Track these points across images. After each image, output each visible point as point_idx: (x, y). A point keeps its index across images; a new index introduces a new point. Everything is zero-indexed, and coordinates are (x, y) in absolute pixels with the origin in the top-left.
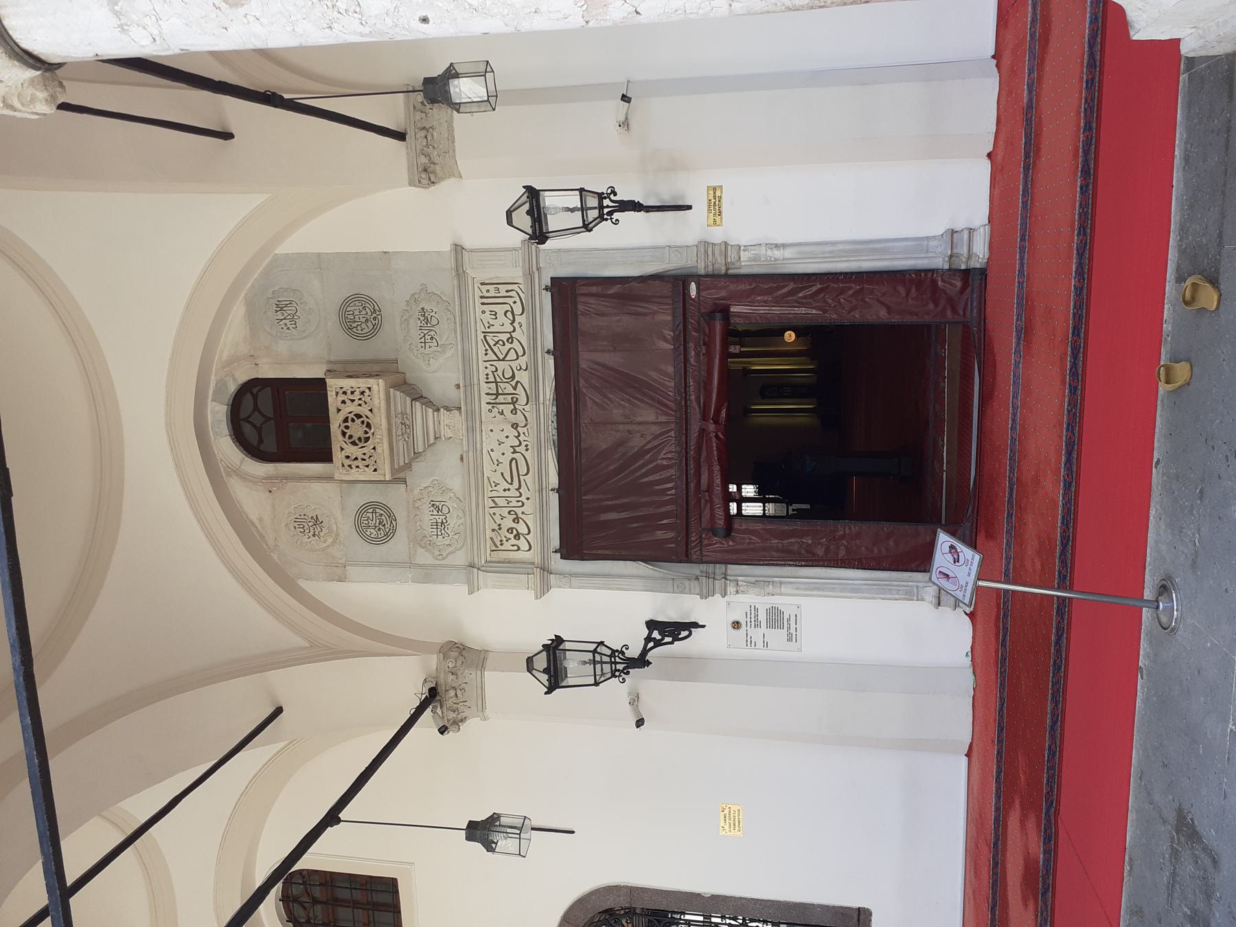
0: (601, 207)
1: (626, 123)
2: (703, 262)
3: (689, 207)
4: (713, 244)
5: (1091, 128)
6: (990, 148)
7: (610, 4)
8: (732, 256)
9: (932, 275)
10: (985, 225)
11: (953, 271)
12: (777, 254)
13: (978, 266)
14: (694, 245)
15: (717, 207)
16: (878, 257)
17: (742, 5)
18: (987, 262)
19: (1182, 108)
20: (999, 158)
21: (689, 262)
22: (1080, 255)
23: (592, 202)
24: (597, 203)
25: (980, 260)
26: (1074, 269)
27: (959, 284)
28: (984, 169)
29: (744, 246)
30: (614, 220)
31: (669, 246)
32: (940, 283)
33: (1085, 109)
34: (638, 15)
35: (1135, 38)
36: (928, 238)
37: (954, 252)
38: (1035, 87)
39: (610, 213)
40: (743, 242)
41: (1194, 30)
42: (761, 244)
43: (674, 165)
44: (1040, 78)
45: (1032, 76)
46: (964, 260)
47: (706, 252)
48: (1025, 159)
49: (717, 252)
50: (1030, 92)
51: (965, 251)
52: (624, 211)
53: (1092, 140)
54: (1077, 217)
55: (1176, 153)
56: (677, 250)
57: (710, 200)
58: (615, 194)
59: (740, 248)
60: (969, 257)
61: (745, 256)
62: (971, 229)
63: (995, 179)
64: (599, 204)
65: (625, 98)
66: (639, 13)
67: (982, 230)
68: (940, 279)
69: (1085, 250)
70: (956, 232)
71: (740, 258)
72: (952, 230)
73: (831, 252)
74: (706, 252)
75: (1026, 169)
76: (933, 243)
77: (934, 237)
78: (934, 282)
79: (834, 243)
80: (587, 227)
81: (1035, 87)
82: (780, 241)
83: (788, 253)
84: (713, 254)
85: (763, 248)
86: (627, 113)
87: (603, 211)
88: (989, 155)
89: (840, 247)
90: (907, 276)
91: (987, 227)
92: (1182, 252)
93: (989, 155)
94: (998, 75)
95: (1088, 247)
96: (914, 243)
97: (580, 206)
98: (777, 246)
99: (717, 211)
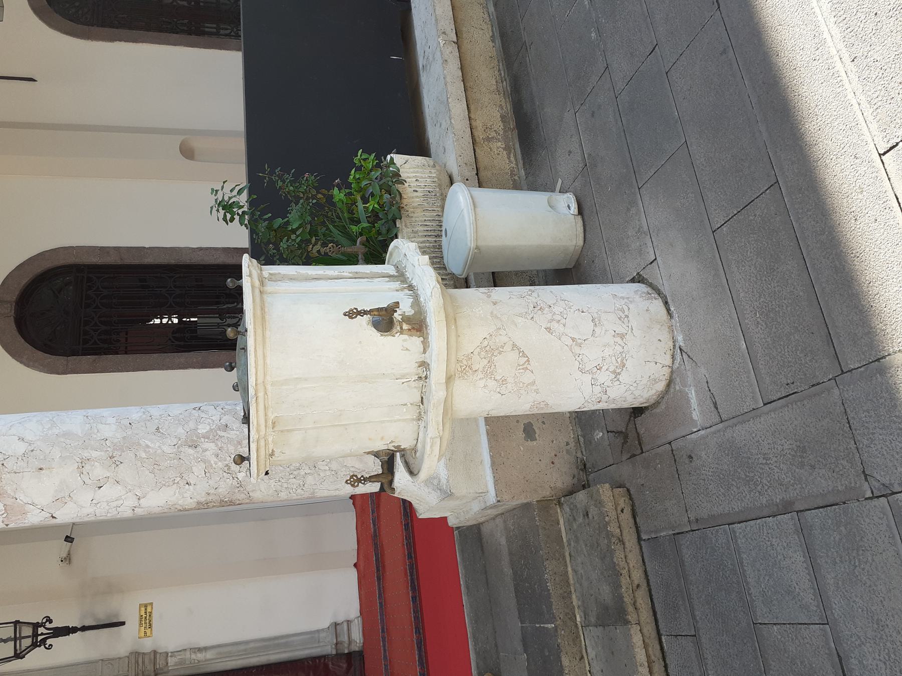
0: (35, 635)
1: (68, 558)
2: (133, 670)
3: (123, 623)
4: (143, 653)
5: (411, 557)
6: (355, 561)
7: (29, 512)
8: (160, 663)
9: (325, 660)
10: (358, 617)
11: (339, 655)
12: (200, 656)
13: (357, 649)
14: (126, 657)
15: (148, 621)
16: (282, 650)
17: (142, 510)
18: (363, 646)
19: (459, 553)
20: (361, 568)
21: (121, 672)
22: (419, 648)
23: (27, 631)
24: (31, 632)
25: (358, 645)
26: (417, 659)
27: (345, 666)
28: (353, 574)
29: (172, 652)
30: (47, 646)
31: (102, 660)
32: (330, 666)
33: (406, 544)
34: (54, 519)
35: (420, 517)
36: (318, 631)
37: (339, 640)
38: (376, 521)
39: (44, 641)
40: (171, 648)
41: (452, 513)
42: (186, 649)
43: (111, 588)
44: (378, 517)
45: (374, 514)
46: (346, 645)
47: (137, 662)
48: (377, 571)
49: (147, 661)
50: (374, 525)
51: (346, 639)
52: (58, 637)
53: (413, 565)
54: (413, 619)
55: (461, 583)
56: (109, 663)
57: (142, 616)
58: (51, 621)
59: (168, 654)
60: (350, 642)
61: (171, 661)
62: (348, 621)
63: (361, 589)
64: (33, 633)
65: (69, 539)
66: (55, 518)
67: (356, 620)
68: (330, 663)
69: (422, 644)
70: (339, 624)
71: (167, 663)
72: (335, 623)
73: (245, 650)
74: (137, 662)
75: (379, 579)
76: (323, 635)
77: (323, 630)
78: (326, 666)
79: (247, 642)
80: (18, 655)
81: (376, 521)
82: (202, 644)
83: (209, 655)
84: (143, 663)
85: (188, 653)
86: (69, 551)
87: (37, 639)
88: (355, 565)
89: (252, 645)
90: (306, 663)
91: (359, 618)
92: (477, 654)
93: (355, 565)
94: (355, 510)
95: (423, 643)
96: (308, 636)
97: (13, 637)
98: (200, 650)
99: (148, 624)
